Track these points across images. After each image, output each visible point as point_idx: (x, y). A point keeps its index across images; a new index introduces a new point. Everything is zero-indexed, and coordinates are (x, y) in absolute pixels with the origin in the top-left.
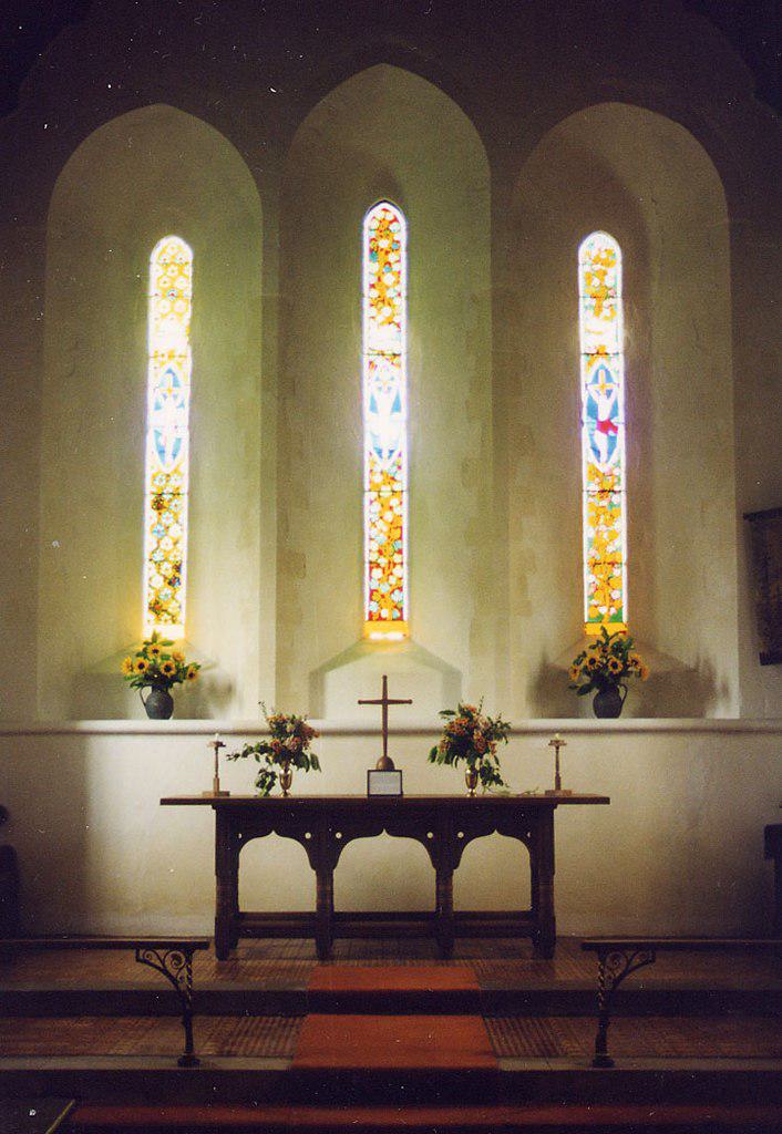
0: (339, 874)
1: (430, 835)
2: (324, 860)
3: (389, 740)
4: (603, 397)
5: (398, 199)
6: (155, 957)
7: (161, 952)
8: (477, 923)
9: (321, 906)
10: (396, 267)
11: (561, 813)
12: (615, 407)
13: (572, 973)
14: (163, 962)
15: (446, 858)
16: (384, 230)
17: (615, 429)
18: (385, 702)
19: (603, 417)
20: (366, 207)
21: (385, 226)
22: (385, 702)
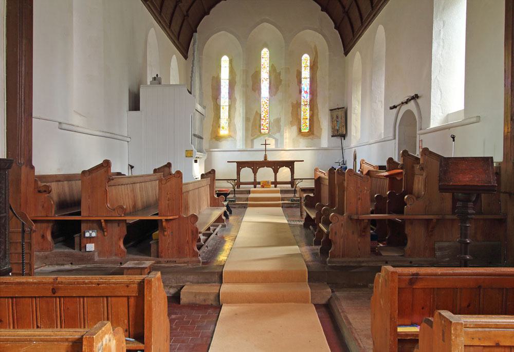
2: (255, 172)
11: (295, 163)
18: (266, 144)
20: (262, 49)
22: (266, 144)
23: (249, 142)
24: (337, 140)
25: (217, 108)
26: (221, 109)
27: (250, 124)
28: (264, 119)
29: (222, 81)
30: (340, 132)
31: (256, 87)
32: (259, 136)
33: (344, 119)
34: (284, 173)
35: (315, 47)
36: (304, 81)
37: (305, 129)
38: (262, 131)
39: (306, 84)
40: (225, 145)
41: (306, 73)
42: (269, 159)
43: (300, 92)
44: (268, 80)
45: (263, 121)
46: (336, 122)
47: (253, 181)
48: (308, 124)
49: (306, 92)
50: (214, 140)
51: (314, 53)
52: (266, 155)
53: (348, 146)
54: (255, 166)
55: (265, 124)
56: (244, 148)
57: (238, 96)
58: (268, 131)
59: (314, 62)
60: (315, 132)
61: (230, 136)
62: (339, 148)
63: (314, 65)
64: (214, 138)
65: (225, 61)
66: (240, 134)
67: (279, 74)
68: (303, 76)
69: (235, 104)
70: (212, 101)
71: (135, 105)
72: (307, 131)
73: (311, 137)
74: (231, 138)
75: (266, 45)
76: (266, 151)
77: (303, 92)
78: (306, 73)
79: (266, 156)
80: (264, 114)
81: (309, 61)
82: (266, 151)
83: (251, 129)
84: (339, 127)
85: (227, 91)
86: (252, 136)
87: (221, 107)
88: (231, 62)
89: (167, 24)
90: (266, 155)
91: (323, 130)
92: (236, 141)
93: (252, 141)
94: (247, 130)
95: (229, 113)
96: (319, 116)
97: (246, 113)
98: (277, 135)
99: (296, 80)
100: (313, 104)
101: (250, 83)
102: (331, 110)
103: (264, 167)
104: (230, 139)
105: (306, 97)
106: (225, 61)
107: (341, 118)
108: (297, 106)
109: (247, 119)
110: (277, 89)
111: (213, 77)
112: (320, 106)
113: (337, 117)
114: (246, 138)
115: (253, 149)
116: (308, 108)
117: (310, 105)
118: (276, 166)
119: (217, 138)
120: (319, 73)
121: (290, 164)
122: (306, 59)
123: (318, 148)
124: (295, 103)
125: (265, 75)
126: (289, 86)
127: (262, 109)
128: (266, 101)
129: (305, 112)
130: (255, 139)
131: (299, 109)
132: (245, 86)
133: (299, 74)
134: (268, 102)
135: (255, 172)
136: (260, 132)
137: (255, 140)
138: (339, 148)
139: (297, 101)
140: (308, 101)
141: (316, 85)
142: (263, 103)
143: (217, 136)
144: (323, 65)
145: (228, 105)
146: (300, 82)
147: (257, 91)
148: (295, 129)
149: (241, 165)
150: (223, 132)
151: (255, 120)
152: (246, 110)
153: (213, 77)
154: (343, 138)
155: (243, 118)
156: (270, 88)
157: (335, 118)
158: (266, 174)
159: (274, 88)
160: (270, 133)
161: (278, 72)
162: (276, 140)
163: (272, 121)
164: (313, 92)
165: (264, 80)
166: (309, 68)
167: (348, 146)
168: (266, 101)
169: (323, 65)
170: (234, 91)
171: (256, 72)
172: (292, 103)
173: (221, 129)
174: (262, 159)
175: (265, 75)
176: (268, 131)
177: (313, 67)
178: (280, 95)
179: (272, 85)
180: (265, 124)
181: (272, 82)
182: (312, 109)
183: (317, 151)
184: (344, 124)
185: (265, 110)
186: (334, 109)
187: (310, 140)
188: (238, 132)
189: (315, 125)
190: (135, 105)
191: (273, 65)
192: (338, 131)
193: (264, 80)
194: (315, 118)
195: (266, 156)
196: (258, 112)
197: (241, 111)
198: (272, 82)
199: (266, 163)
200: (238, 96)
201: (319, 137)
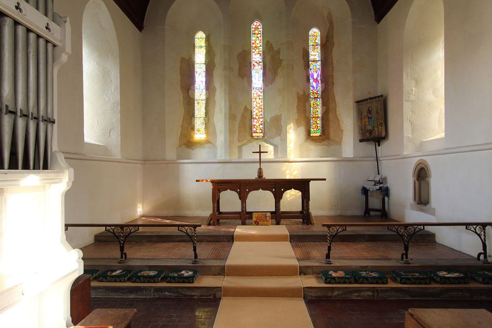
0: (282, 202)
1: (247, 190)
2: (243, 198)
3: (261, 164)
4: (315, 73)
5: (261, 21)
6: (472, 228)
7: (186, 228)
8: (287, 215)
9: (242, 210)
10: (260, 38)
11: (311, 183)
12: (318, 75)
13: (317, 229)
14: (475, 229)
15: (278, 197)
16: (256, 28)
17: (318, 81)
18: (260, 152)
19: (315, 78)
20: (252, 22)
21: (257, 26)
22: (260, 152)
23: (236, 150)
24: (369, 147)
25: (190, 103)
26: (196, 104)
27: (237, 123)
28: (257, 117)
29: (196, 65)
30: (376, 134)
31: (245, 72)
32: (250, 142)
33: (381, 113)
34: (292, 197)
35: (330, 14)
36: (312, 65)
37: (316, 133)
38: (254, 135)
39: (315, 69)
40: (201, 154)
41: (315, 54)
42: (268, 175)
43: (308, 80)
44: (261, 64)
45: (255, 120)
46: (367, 120)
47: (240, 210)
48: (319, 125)
49: (316, 80)
50: (184, 147)
51: (328, 25)
52: (260, 169)
53: (399, 155)
54: (243, 187)
55: (257, 124)
56: (228, 159)
57: (217, 83)
58: (262, 135)
59: (327, 37)
60: (332, 135)
61: (207, 142)
62: (373, 159)
63: (327, 41)
64: (185, 144)
65: (200, 38)
66: (221, 138)
67: (279, 52)
68: (311, 58)
69: (214, 96)
70: (180, 91)
71: (197, 181)
72: (318, 134)
73: (325, 142)
74: (209, 144)
75: (258, 17)
76: (260, 162)
77: (311, 81)
78: (315, 54)
79: (260, 172)
80: (257, 111)
81: (319, 38)
82: (260, 162)
83: (237, 130)
84: (373, 127)
85: (204, 79)
86: (239, 141)
87: (196, 102)
88: (208, 40)
89: (139, 29)
90: (260, 169)
91: (345, 133)
92: (217, 148)
93: (240, 148)
94: (231, 131)
95: (206, 109)
96: (337, 113)
97: (230, 108)
98: (277, 140)
99: (302, 62)
100: (327, 97)
101: (236, 67)
102: (357, 102)
103: (291, 189)
104: (206, 146)
105: (316, 87)
106: (200, 38)
107: (377, 113)
108: (304, 99)
109: (232, 117)
110: (275, 73)
111: (183, 59)
112: (338, 99)
113: (370, 112)
114: (230, 144)
115: (240, 160)
116: (319, 102)
117: (323, 97)
118: (279, 187)
119: (188, 143)
120: (336, 52)
121: (302, 185)
122: (315, 34)
123: (340, 159)
124: (301, 93)
125: (256, 57)
126: (293, 69)
127: (254, 104)
128: (259, 93)
129: (317, 108)
130: (244, 145)
131: (307, 104)
132: (228, 68)
133: (306, 54)
134: (262, 94)
135: (243, 198)
136: (252, 136)
137: (244, 148)
138: (373, 159)
139: (304, 92)
140: (320, 92)
141: (330, 69)
142: (255, 95)
143: (189, 142)
144: (344, 42)
145: (205, 98)
146: (307, 66)
147: (246, 78)
148: (302, 130)
149: (220, 186)
150: (199, 135)
151: (243, 117)
152: (230, 103)
153: (183, 59)
154: (377, 144)
155: (225, 114)
156: (264, 74)
157: (365, 113)
158: (261, 201)
159: (269, 75)
160: (266, 137)
161: (275, 49)
162: (276, 147)
163: (268, 120)
164: (327, 79)
165: (255, 64)
166: (319, 47)
167: (399, 155)
168: (259, 93)
169: (344, 42)
170: (213, 77)
171: (244, 51)
172: (298, 93)
173: (196, 132)
174: (254, 176)
175: (256, 57)
176: (262, 135)
177: (326, 46)
178: (279, 81)
179: (267, 69)
180: (257, 124)
181: (268, 66)
182: (325, 103)
183: (337, 163)
184: (382, 121)
185: (258, 105)
186: (363, 100)
187: (325, 146)
188: (218, 137)
189: (332, 126)
190: (197, 181)
191: (268, 42)
192: (371, 132)
193: (255, 64)
194: (331, 116)
195: (260, 172)
196: (249, 108)
197: (223, 104)
198: (268, 66)
199: (261, 183)
200: (218, 73)
201: (339, 143)
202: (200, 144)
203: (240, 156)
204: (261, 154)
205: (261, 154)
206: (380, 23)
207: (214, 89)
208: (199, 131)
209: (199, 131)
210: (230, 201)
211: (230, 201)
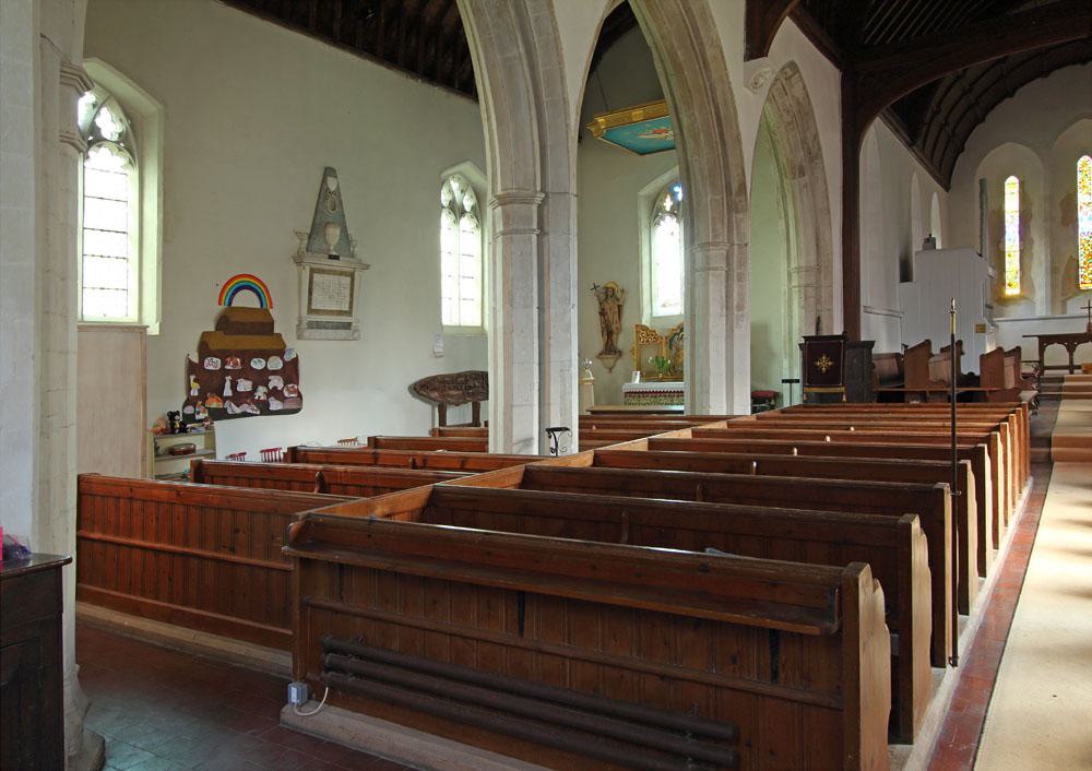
2: (1071, 350)
27: (1060, 277)
32: (1076, 294)
40: (1014, 311)
56: (1049, 314)
57: (1036, 235)
61: (1021, 298)
65: (1012, 186)
66: (1041, 294)
69: (1031, 248)
88: (1022, 185)
93: (1064, 303)
94: (1053, 286)
97: (1052, 262)
101: (1059, 214)
104: (1023, 302)
106: (1012, 186)
109: (1053, 270)
127: (1081, 252)
130: (1069, 298)
135: (1071, 350)
137: (1069, 302)
143: (1000, 298)
149: (1045, 340)
150: (1012, 290)
155: (1046, 269)
171: (1070, 195)
197: (1043, 257)
200: (1036, 235)
202: (1012, 300)
203: (1064, 312)
204: (1068, 363)
205: (1068, 363)
206: (970, 612)
207: (1031, 242)
208: (1010, 285)
209: (1010, 285)
210: (1057, 354)
211: (1057, 354)
